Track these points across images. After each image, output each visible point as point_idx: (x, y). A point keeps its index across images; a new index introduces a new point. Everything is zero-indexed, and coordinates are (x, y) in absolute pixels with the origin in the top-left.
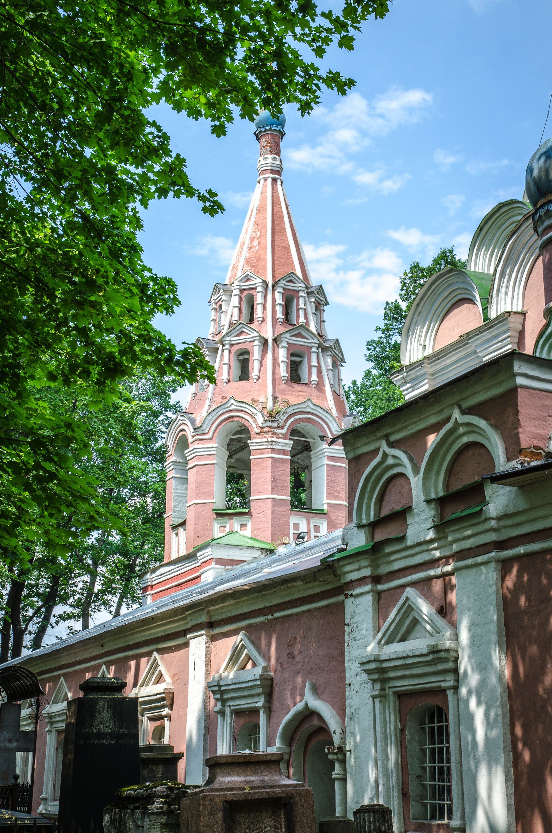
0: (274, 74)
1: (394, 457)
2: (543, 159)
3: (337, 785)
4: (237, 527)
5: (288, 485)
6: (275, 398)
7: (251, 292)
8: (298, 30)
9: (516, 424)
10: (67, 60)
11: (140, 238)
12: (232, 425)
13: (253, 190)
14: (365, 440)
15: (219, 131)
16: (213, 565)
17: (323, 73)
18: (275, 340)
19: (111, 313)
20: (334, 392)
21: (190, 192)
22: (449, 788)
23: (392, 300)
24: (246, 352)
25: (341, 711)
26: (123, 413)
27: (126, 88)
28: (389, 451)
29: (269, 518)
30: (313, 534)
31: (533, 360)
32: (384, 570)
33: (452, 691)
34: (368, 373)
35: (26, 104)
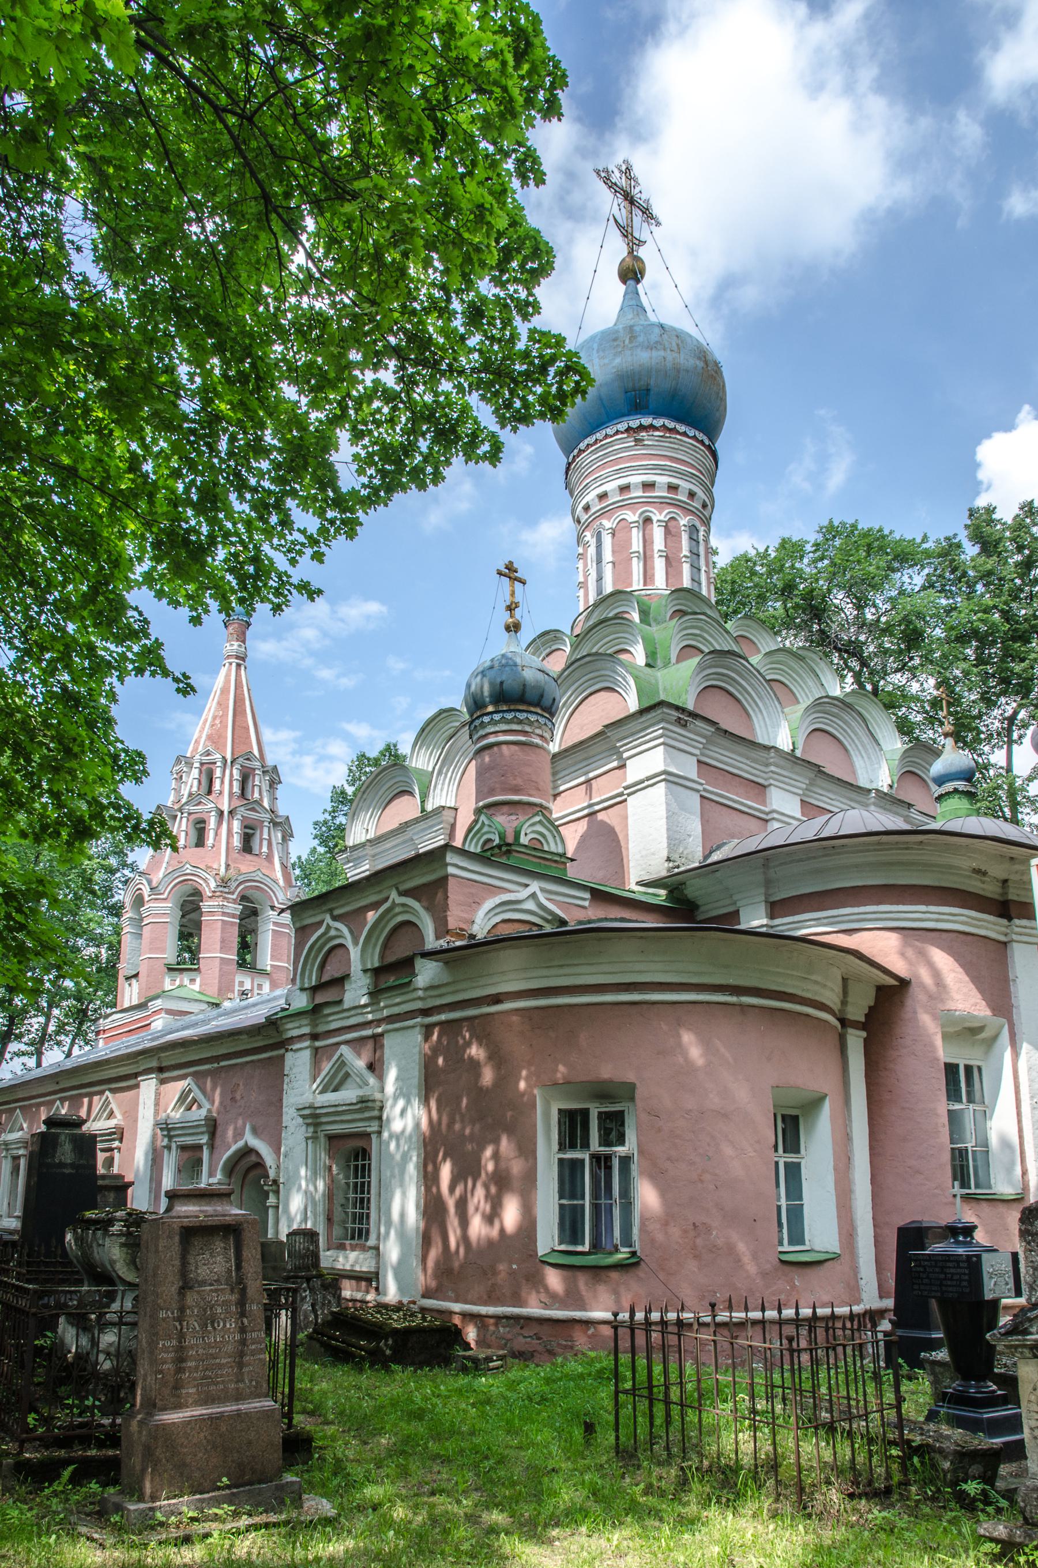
0: (251, 576)
1: (337, 929)
2: (479, 678)
3: (271, 1212)
4: (186, 982)
5: (235, 946)
6: (228, 866)
8: (275, 541)
9: (445, 908)
10: (57, 541)
11: (115, 711)
12: (187, 888)
13: (218, 673)
14: (311, 912)
15: (196, 621)
16: (163, 1015)
17: (295, 580)
18: (230, 812)
19: (85, 781)
20: (282, 864)
21: (166, 673)
22: (368, 1216)
23: (338, 784)
24: (203, 821)
25: (277, 1151)
26: (85, 870)
27: (112, 574)
28: (332, 923)
29: (217, 975)
30: (256, 991)
31: (462, 852)
32: (322, 1028)
34: (314, 851)
35: (15, 578)
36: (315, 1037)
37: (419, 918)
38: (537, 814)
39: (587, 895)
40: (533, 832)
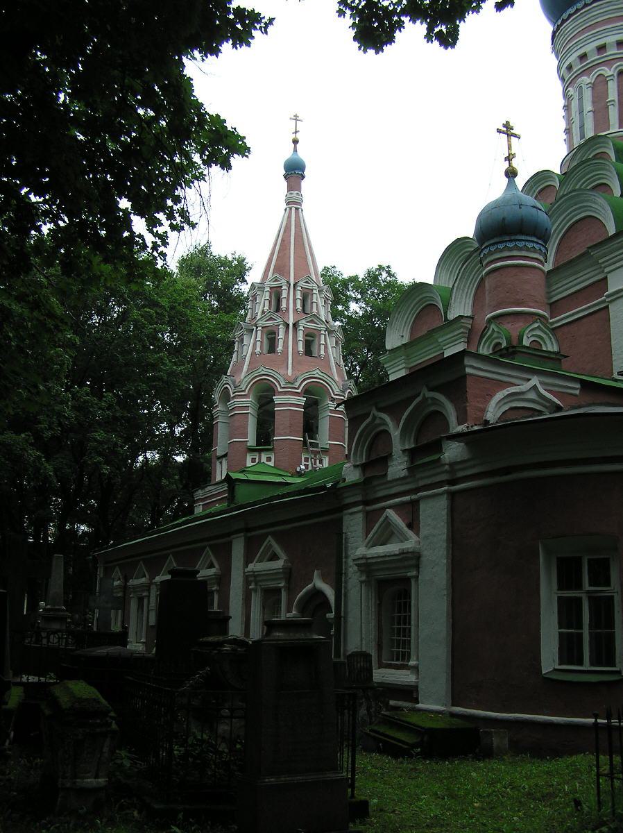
7: (278, 289)
18: (294, 325)
22: (410, 641)
28: (377, 413)
33: (414, 580)
36: (366, 503)
37: (444, 407)
38: (536, 322)
39: (578, 386)
40: (533, 336)
